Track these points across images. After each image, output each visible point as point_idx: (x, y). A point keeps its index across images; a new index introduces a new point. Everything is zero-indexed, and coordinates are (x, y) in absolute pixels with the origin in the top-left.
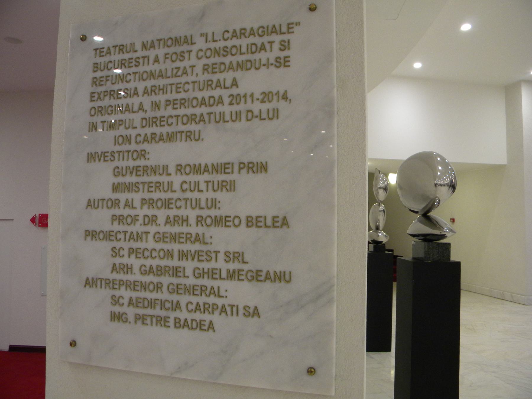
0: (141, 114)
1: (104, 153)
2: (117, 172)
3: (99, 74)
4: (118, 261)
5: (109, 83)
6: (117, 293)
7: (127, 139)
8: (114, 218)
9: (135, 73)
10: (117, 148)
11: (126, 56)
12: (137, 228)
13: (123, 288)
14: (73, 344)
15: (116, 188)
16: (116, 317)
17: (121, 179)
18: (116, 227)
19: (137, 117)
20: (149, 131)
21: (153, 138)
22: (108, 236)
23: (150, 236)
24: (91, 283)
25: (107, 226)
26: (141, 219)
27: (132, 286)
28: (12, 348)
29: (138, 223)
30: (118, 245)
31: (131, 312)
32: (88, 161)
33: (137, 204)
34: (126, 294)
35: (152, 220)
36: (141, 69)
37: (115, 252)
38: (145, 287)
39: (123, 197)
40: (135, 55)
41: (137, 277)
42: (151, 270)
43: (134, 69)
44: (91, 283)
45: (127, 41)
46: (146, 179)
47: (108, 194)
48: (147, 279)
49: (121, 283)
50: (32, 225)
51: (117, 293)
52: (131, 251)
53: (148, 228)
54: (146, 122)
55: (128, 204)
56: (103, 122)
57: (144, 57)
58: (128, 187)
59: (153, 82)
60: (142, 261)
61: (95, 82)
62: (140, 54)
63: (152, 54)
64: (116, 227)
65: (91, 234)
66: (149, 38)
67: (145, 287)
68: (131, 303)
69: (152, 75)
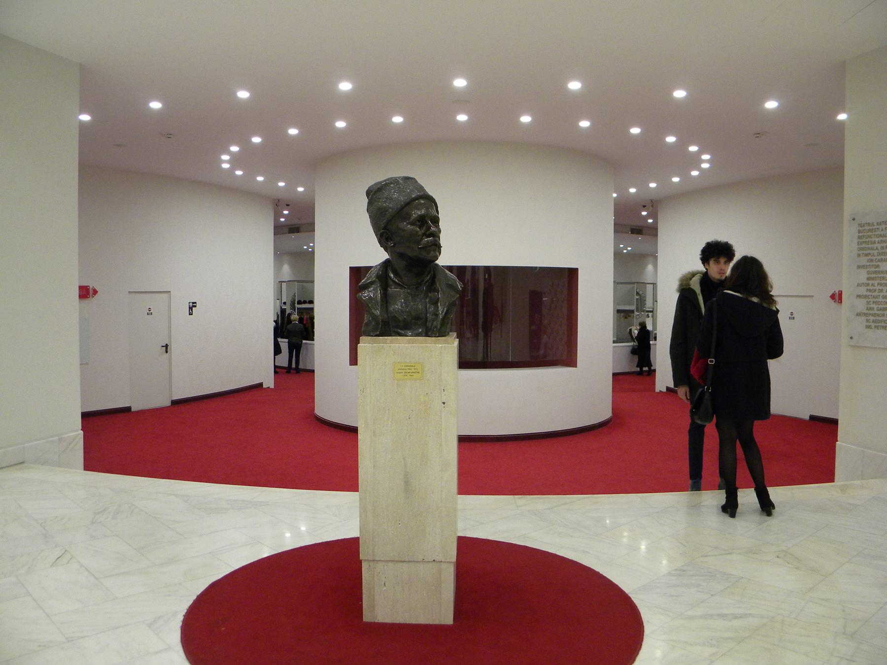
0: (877, 251)
1: (863, 266)
2: (869, 273)
3: (860, 234)
4: (869, 306)
5: (864, 238)
6: (869, 318)
7: (872, 261)
8: (867, 290)
9: (874, 235)
10: (868, 264)
11: (871, 228)
12: (876, 294)
13: (870, 316)
14: (851, 338)
15: (868, 279)
16: (868, 327)
17: (870, 276)
18: (868, 293)
19: (876, 252)
20: (880, 257)
21: (881, 260)
22: (865, 297)
23: (881, 297)
24: (858, 314)
25: (865, 293)
26: (877, 290)
27: (874, 315)
28: (813, 418)
29: (876, 292)
30: (869, 300)
31: (873, 325)
32: (858, 268)
33: (876, 284)
34: (871, 318)
35: (881, 291)
36: (876, 233)
37: (868, 303)
38: (878, 315)
39: (871, 282)
40: (874, 227)
41: (876, 312)
42: (881, 309)
43: (874, 233)
44: (858, 314)
45: (871, 222)
46: (879, 276)
47: (865, 281)
48: (879, 312)
49: (870, 314)
50: (832, 301)
51: (869, 318)
52: (874, 302)
53: (880, 294)
54: (879, 254)
55: (873, 285)
56: (863, 254)
57: (877, 228)
58: (873, 279)
59: (881, 238)
60: (877, 306)
61: (859, 237)
62: (876, 227)
63: (880, 227)
64: (868, 293)
65: (859, 296)
66: (879, 221)
67: (878, 315)
68: (873, 321)
69: (881, 236)
